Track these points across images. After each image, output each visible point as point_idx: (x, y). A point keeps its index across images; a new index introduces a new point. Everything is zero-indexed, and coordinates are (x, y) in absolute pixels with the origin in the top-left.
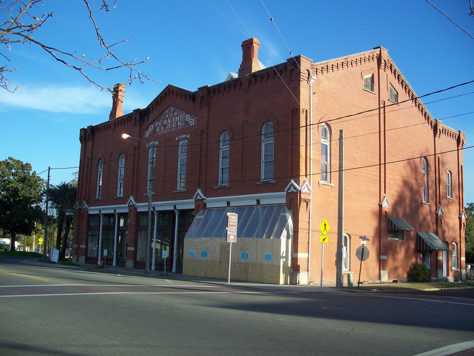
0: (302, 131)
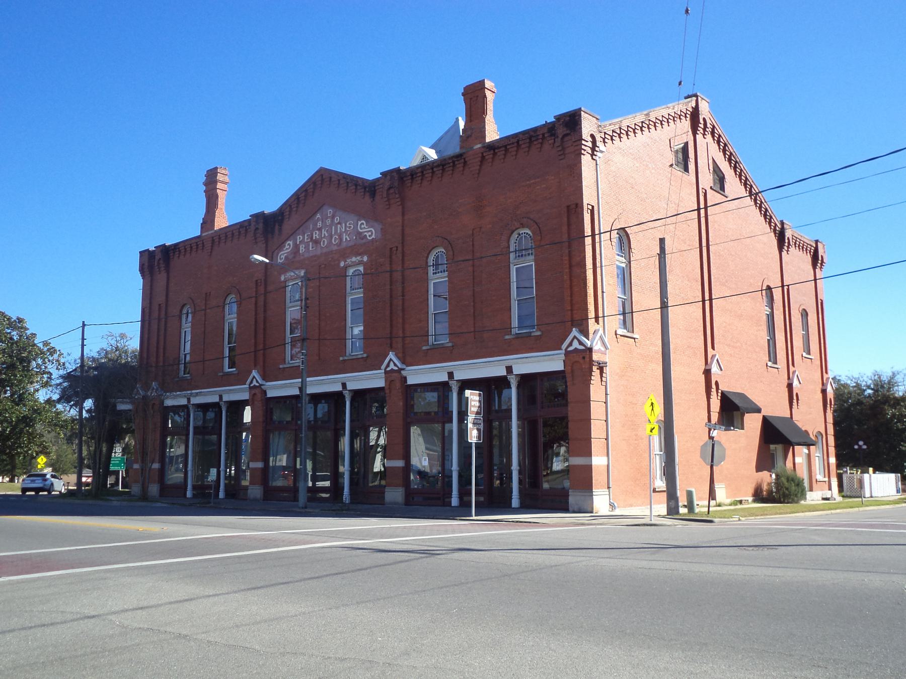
0: (588, 241)
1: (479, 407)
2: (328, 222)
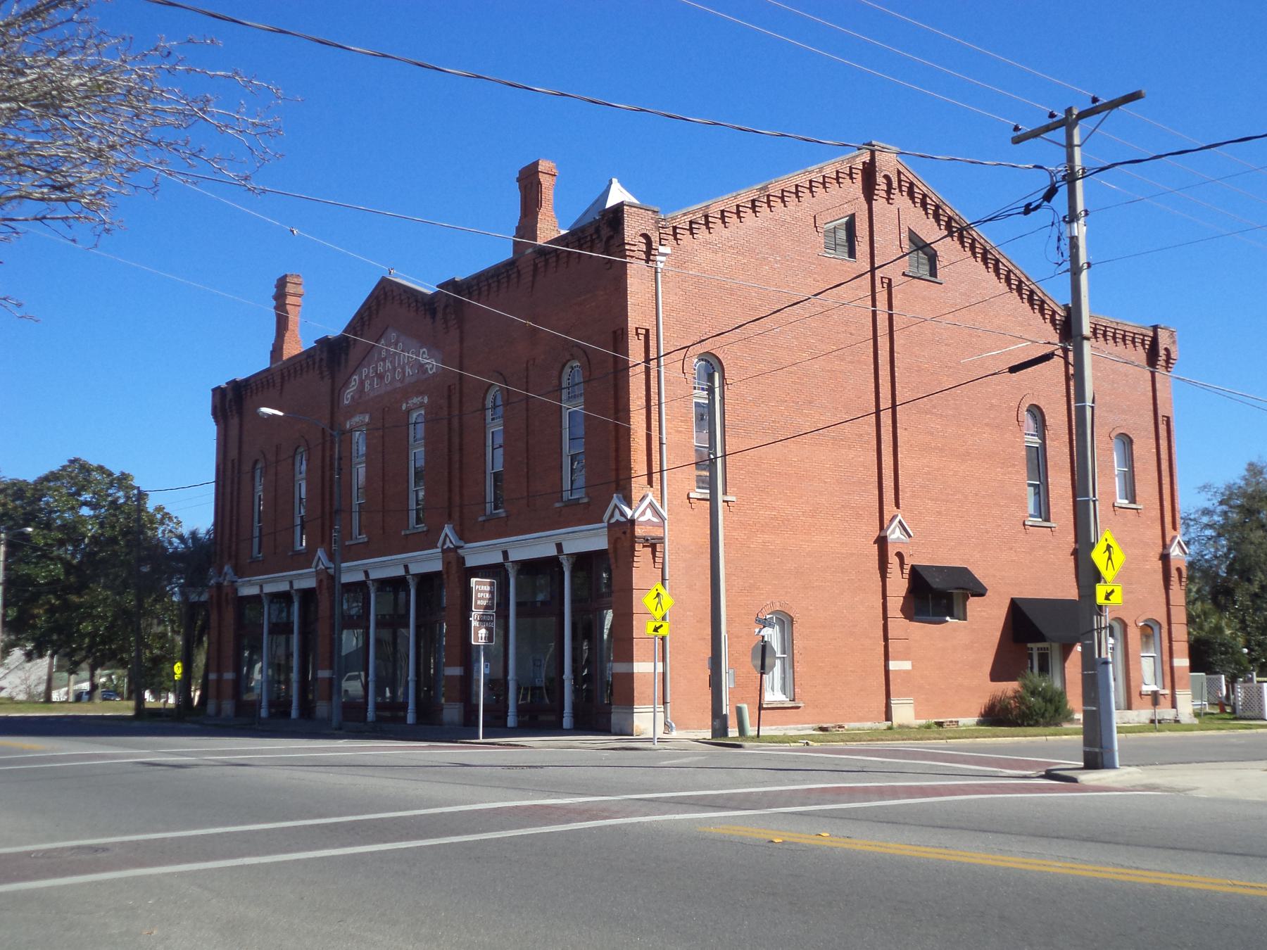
1: (489, 599)
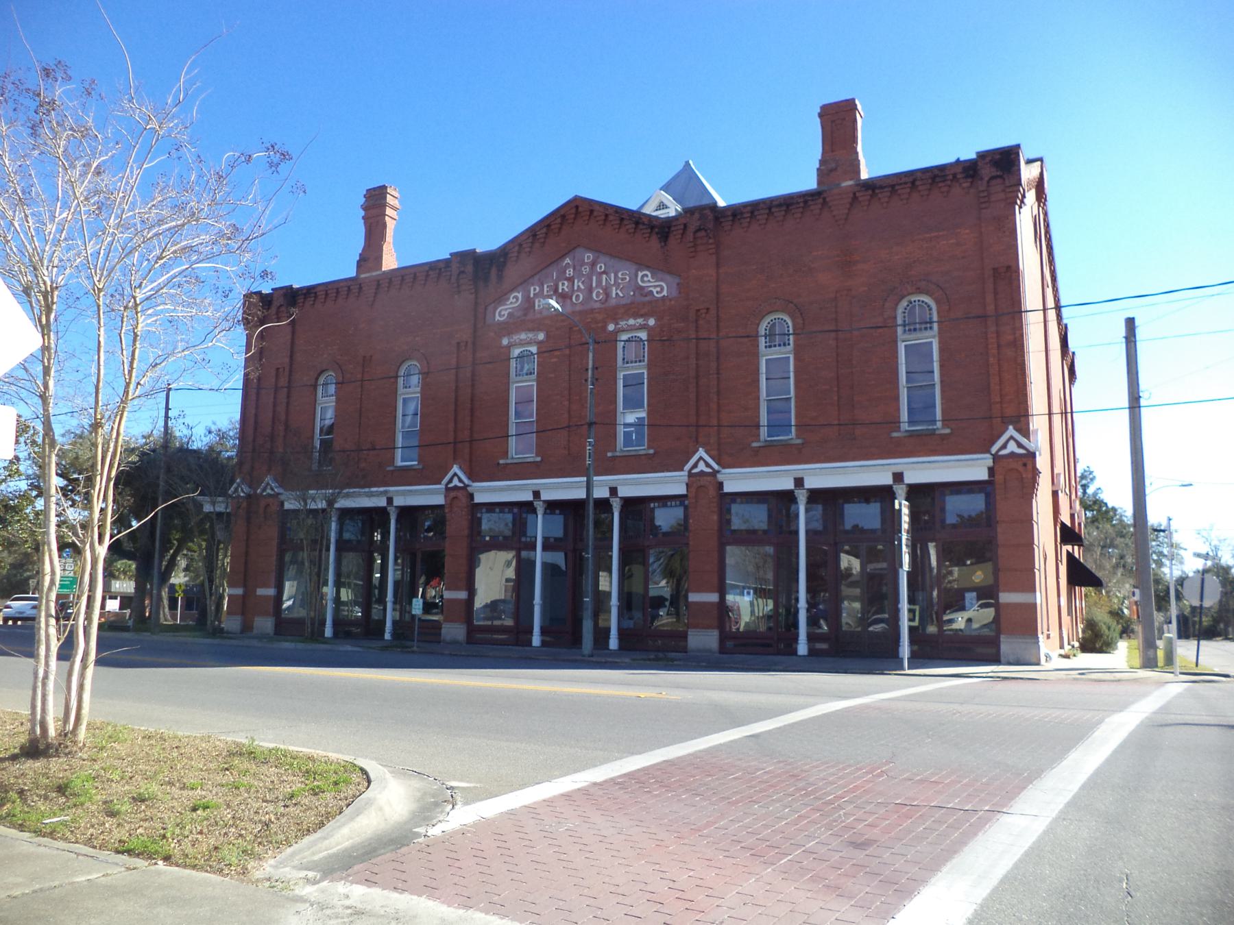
2: (586, 270)
